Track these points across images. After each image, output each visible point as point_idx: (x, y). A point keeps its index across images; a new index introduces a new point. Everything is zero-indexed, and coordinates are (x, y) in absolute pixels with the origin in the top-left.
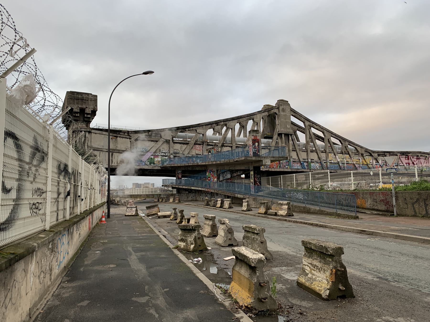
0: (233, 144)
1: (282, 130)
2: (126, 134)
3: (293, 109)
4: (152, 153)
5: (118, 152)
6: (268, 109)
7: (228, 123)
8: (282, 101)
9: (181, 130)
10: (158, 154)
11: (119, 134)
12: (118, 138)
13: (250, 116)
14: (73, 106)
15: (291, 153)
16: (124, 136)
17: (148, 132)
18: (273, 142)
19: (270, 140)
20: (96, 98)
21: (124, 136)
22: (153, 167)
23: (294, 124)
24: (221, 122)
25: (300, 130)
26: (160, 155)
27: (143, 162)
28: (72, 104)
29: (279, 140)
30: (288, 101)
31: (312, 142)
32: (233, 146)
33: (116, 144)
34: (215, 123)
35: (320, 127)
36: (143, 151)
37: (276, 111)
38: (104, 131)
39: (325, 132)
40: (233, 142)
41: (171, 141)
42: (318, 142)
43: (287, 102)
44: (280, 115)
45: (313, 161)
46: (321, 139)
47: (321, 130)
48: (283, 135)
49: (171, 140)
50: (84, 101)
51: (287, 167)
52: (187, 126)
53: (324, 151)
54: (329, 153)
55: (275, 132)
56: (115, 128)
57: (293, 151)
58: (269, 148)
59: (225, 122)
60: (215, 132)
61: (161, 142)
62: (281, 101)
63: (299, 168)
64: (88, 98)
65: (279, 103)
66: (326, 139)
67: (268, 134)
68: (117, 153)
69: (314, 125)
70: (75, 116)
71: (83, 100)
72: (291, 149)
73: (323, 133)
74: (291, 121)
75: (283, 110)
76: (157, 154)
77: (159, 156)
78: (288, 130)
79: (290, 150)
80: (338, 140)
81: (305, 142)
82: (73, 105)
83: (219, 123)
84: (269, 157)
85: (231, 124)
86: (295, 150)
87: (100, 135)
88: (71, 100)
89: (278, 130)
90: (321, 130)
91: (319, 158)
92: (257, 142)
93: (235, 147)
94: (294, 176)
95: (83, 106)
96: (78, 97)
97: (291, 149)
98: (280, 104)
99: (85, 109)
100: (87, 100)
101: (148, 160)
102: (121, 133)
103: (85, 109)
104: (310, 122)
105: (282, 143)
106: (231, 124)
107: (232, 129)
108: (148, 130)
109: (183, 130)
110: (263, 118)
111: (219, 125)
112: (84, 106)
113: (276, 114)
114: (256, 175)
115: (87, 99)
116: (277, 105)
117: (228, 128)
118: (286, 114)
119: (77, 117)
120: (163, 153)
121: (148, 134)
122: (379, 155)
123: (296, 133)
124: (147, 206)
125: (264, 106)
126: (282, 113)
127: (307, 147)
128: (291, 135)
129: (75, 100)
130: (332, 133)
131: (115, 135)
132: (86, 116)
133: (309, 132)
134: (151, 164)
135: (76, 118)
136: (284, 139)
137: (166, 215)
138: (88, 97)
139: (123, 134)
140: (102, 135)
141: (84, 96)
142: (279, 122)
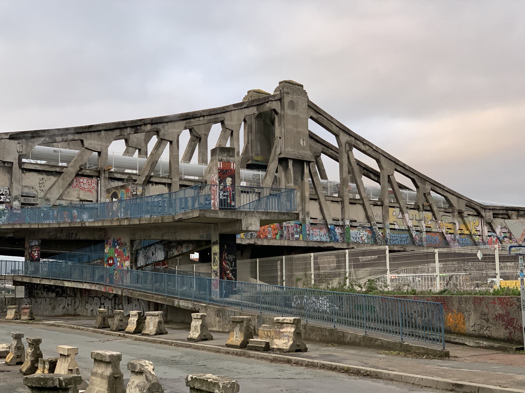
0: (174, 180)
8: (289, 84)
13: (215, 114)
15: (307, 205)
18: (268, 177)
19: (261, 173)
23: (316, 138)
24: (145, 124)
29: (281, 175)
30: (302, 86)
31: (354, 180)
32: (173, 184)
34: (131, 127)
35: (372, 148)
37: (275, 105)
39: (382, 159)
40: (172, 174)
41: (16, 166)
42: (367, 183)
43: (301, 87)
44: (284, 115)
45: (354, 224)
47: (373, 154)
48: (290, 163)
51: (297, 236)
53: (379, 203)
54: (390, 207)
57: (311, 199)
59: (155, 126)
60: (131, 149)
62: (286, 84)
65: (283, 88)
67: (256, 158)
72: (307, 194)
73: (378, 161)
78: (302, 152)
79: (305, 197)
83: (140, 126)
85: (170, 131)
86: (316, 197)
89: (278, 151)
90: (373, 154)
91: (368, 218)
97: (307, 194)
98: (285, 90)
104: (350, 135)
105: (287, 180)
106: (170, 131)
107: (171, 142)
110: (245, 121)
111: (140, 131)
113: (277, 113)
117: (162, 139)
118: (298, 113)
122: (495, 216)
123: (320, 159)
125: (249, 92)
126: (289, 112)
128: (309, 163)
142: (281, 131)
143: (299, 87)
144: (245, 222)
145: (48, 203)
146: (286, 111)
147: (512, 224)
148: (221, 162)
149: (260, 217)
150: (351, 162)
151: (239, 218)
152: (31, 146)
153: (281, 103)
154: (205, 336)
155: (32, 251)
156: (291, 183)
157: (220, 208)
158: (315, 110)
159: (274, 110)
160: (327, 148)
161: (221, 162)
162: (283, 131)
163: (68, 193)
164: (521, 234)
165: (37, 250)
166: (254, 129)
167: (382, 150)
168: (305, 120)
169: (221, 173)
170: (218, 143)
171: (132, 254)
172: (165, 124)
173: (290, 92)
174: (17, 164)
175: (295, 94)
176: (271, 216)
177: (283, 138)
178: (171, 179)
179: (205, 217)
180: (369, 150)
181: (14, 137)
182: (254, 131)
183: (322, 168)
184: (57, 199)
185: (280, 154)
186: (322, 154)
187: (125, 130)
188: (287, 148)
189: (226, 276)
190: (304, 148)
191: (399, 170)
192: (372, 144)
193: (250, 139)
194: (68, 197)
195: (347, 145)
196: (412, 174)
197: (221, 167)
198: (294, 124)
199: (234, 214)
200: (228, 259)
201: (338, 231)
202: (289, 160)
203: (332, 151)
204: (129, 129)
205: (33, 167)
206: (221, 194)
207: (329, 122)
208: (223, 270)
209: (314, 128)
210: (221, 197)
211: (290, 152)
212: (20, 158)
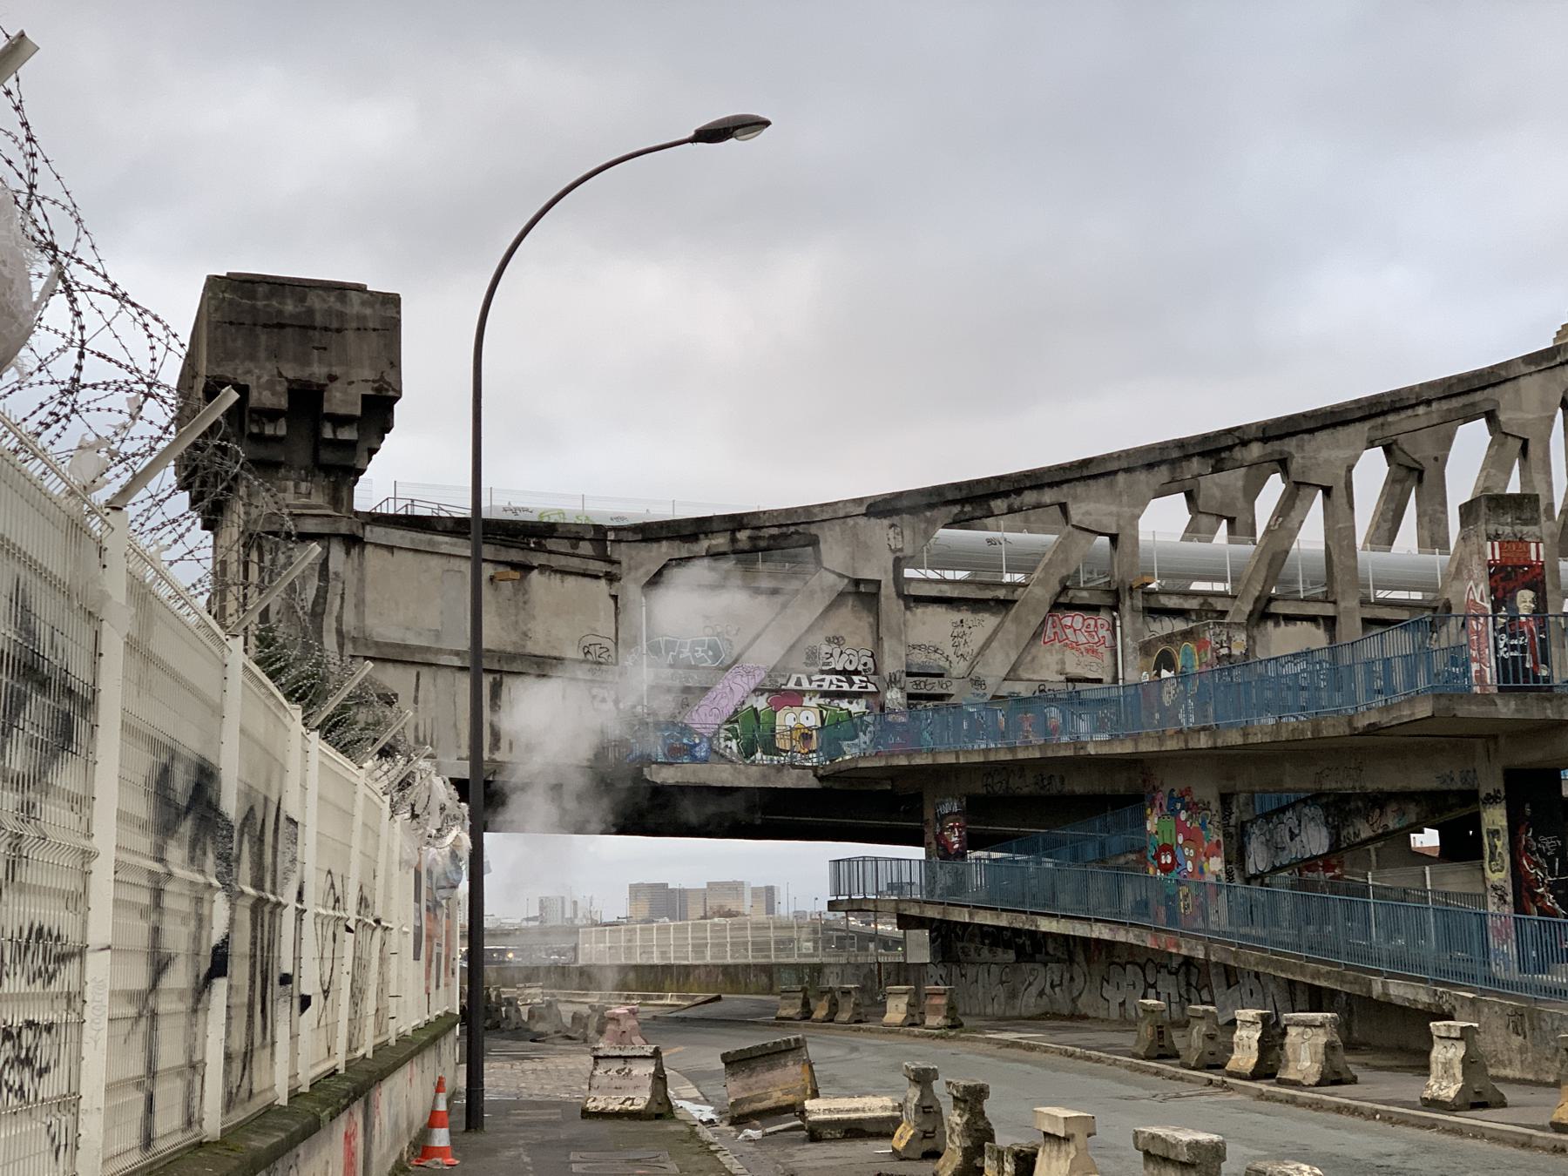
0: (1342, 605)
2: (586, 548)
4: (760, 676)
7: (1300, 447)
10: (799, 683)
11: (541, 548)
12: (535, 574)
14: (249, 372)
16: (575, 563)
17: (733, 531)
21: (575, 563)
22: (764, 776)
24: (1245, 443)
26: (814, 686)
28: (242, 362)
32: (1342, 620)
34: (1202, 454)
41: (888, 590)
56: (515, 511)
60: (1205, 521)
64: (341, 315)
71: (311, 333)
76: (791, 685)
77: (802, 693)
82: (251, 365)
83: (1230, 448)
85: (1324, 454)
93: (1359, 624)
96: (280, 312)
100: (339, 331)
101: (729, 721)
102: (551, 544)
103: (321, 389)
107: (1327, 492)
109: (968, 508)
111: (1229, 464)
112: (317, 371)
115: (335, 325)
117: (1298, 484)
120: (834, 677)
121: (734, 540)
124: (731, 1049)
129: (259, 329)
131: (514, 555)
132: (328, 433)
134: (748, 751)
137: (859, 1120)
138: (338, 306)
139: (570, 551)
140: (434, 562)
141: (315, 301)
145: (981, 692)
148: (1496, 544)
157: (1500, 689)
161: (1496, 544)
163: (1033, 659)
165: (958, 827)
170: (1481, 482)
171: (1226, 835)
172: (1306, 437)
174: (892, 582)
178: (1335, 602)
179: (1454, 716)
181: (883, 508)
184: (1005, 680)
187: (1184, 463)
194: (1034, 673)
197: (1497, 557)
200: (1539, 850)
204: (1195, 460)
210: (1501, 653)
212: (898, 564)
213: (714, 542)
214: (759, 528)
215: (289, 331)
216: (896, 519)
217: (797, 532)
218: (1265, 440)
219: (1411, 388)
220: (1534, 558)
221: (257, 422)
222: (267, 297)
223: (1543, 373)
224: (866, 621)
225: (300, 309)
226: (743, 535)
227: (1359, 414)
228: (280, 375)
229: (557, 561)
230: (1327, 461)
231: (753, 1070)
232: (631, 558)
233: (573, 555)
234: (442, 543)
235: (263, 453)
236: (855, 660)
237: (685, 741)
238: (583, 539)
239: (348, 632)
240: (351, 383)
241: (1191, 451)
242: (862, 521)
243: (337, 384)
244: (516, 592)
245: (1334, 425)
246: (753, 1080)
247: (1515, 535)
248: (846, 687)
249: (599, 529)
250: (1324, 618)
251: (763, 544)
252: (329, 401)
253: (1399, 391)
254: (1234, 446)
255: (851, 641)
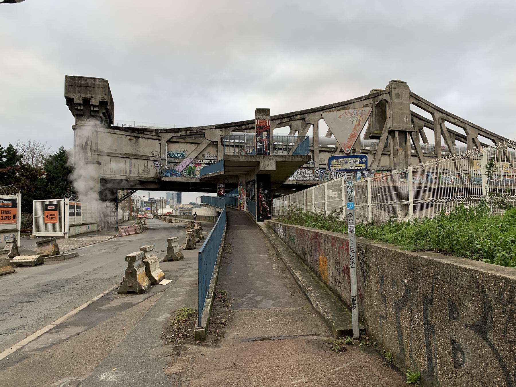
0: (315, 147)
1: (395, 126)
2: (154, 134)
3: (415, 94)
4: (191, 160)
5: (140, 158)
6: (375, 95)
7: (308, 116)
8: (396, 83)
9: (235, 127)
10: (200, 161)
11: (144, 134)
12: (140, 139)
13: (343, 105)
14: (74, 96)
16: (150, 137)
17: (186, 131)
18: (380, 143)
19: (376, 141)
20: (106, 84)
21: (150, 137)
22: (188, 180)
23: (420, 117)
24: (296, 115)
25: (428, 126)
26: (203, 162)
27: (178, 172)
28: (72, 93)
29: (391, 141)
30: (405, 83)
32: (315, 150)
33: (137, 146)
34: (287, 117)
35: (459, 120)
36: (179, 157)
37: (386, 97)
38: (123, 130)
39: (468, 127)
40: (314, 144)
41: (219, 143)
42: (458, 144)
43: (405, 84)
44: (392, 103)
45: (445, 171)
46: (460, 137)
47: (461, 124)
48: (397, 133)
49: (219, 141)
50: (89, 88)
51: (401, 180)
52: (244, 121)
55: (384, 128)
56: (142, 126)
57: (412, 156)
58: (373, 152)
59: (303, 116)
60: (293, 131)
61: (204, 144)
62: (394, 82)
63: (423, 182)
64: (94, 84)
65: (391, 85)
66: (469, 139)
67: (376, 132)
68: (139, 160)
69: (448, 116)
70: (77, 109)
71: (88, 88)
73: (465, 129)
74: (411, 111)
75: (398, 96)
76: (199, 162)
77: (201, 164)
78: (405, 126)
79: (408, 154)
80: (491, 140)
81: (434, 144)
82: (74, 94)
83: (293, 116)
84: (273, 156)
85: (313, 118)
86: (417, 155)
87: (111, 134)
88: (70, 87)
89: (388, 126)
90: (461, 124)
91: (457, 168)
92: (265, 131)
93: (318, 151)
94: (313, 190)
95: (87, 96)
96: (81, 83)
98: (393, 86)
99: (90, 99)
100: (94, 87)
101: (185, 169)
102: (146, 133)
103: (90, 99)
104: (442, 113)
105: (395, 144)
106: (313, 118)
107: (313, 125)
108: (186, 128)
109: (237, 127)
111: (293, 119)
112: (89, 96)
113: (387, 102)
114: (261, 190)
115: (93, 86)
116: (388, 88)
117: (307, 123)
118: (402, 101)
119: (80, 110)
120: (208, 161)
121: (186, 133)
123: (423, 130)
124: (38, 241)
125: (371, 91)
126: (395, 100)
127: (437, 152)
128: (410, 133)
129: (76, 87)
130: (479, 130)
131: (135, 135)
132: (92, 109)
133: (441, 128)
134: (190, 175)
135: (79, 113)
136: (398, 139)
137: (21, 262)
138: (94, 82)
139: (150, 134)
140: (115, 135)
141: (88, 81)
142: (390, 113)
143: (404, 84)
144: (262, 163)
146: (393, 100)
147: (334, 119)
148: (258, 121)
149: (275, 159)
150: (444, 130)
151: (258, 161)
152: (228, 132)
153: (390, 95)
154: (171, 257)
155: (220, 190)
156: (397, 146)
157: (257, 154)
158: (415, 98)
159: (385, 100)
160: (428, 123)
161: (258, 121)
162: (391, 113)
164: (349, 135)
166: (375, 114)
167: (468, 121)
168: (408, 105)
169: (258, 129)
171: (246, 191)
172: (309, 114)
173: (396, 87)
174: (220, 142)
175: (400, 88)
176: (286, 159)
177: (391, 117)
178: (314, 147)
179: (229, 160)
180: (457, 122)
181: (219, 127)
182: (375, 115)
183: (425, 136)
185: (389, 128)
186: (424, 127)
187: (283, 119)
188: (394, 124)
189: (262, 206)
190: (407, 123)
191: (482, 134)
192: (460, 118)
193: (372, 120)
195: (440, 119)
196: (492, 136)
197: (258, 124)
198: (399, 108)
199: (253, 158)
200: (264, 193)
201: (433, 176)
202: (396, 132)
203: (432, 125)
204: (286, 118)
205: (230, 144)
206: (258, 145)
207: (426, 105)
208: (260, 201)
209: (415, 109)
210: (258, 147)
211: (396, 126)
212: (222, 139)
213: (182, 133)
214: (192, 130)
215: (83, 87)
216: (221, 129)
217: (200, 132)
218: (301, 114)
219: (332, 104)
220: (267, 124)
221: (76, 106)
222: (78, 80)
223: (360, 102)
224: (215, 149)
225: (85, 83)
226: (188, 132)
227: (320, 109)
228: (81, 96)
229: (147, 136)
230: (313, 119)
231: (43, 246)
232: (164, 136)
233: (151, 135)
234: (117, 132)
235: (79, 113)
236: (213, 157)
237: (175, 173)
238: (153, 132)
239: (93, 149)
240: (96, 98)
241: (285, 116)
242: (214, 130)
243: (93, 98)
244: (136, 142)
245: (315, 112)
246: (42, 248)
247: (263, 119)
248: (210, 163)
249: (156, 130)
250: (312, 150)
251: (193, 134)
252: (92, 102)
253: (329, 105)
254: (294, 115)
255: (212, 153)
